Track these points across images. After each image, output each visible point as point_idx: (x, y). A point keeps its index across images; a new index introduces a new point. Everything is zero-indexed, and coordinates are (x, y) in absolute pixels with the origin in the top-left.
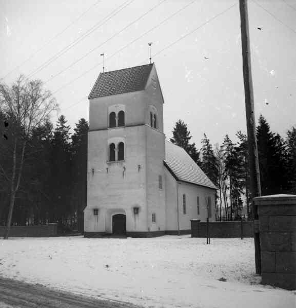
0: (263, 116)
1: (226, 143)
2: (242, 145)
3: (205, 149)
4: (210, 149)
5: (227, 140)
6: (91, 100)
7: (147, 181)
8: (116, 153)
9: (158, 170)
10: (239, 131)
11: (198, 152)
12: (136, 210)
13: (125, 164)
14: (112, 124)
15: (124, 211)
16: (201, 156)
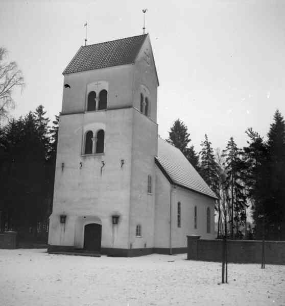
0: (279, 112)
1: (230, 147)
2: (252, 145)
3: (204, 153)
4: (211, 153)
5: (232, 143)
6: (67, 76)
7: (131, 182)
8: (94, 144)
9: (148, 168)
10: (249, 127)
11: (197, 155)
12: (116, 219)
13: (103, 158)
14: (91, 107)
15: (100, 220)
16: (200, 161)
